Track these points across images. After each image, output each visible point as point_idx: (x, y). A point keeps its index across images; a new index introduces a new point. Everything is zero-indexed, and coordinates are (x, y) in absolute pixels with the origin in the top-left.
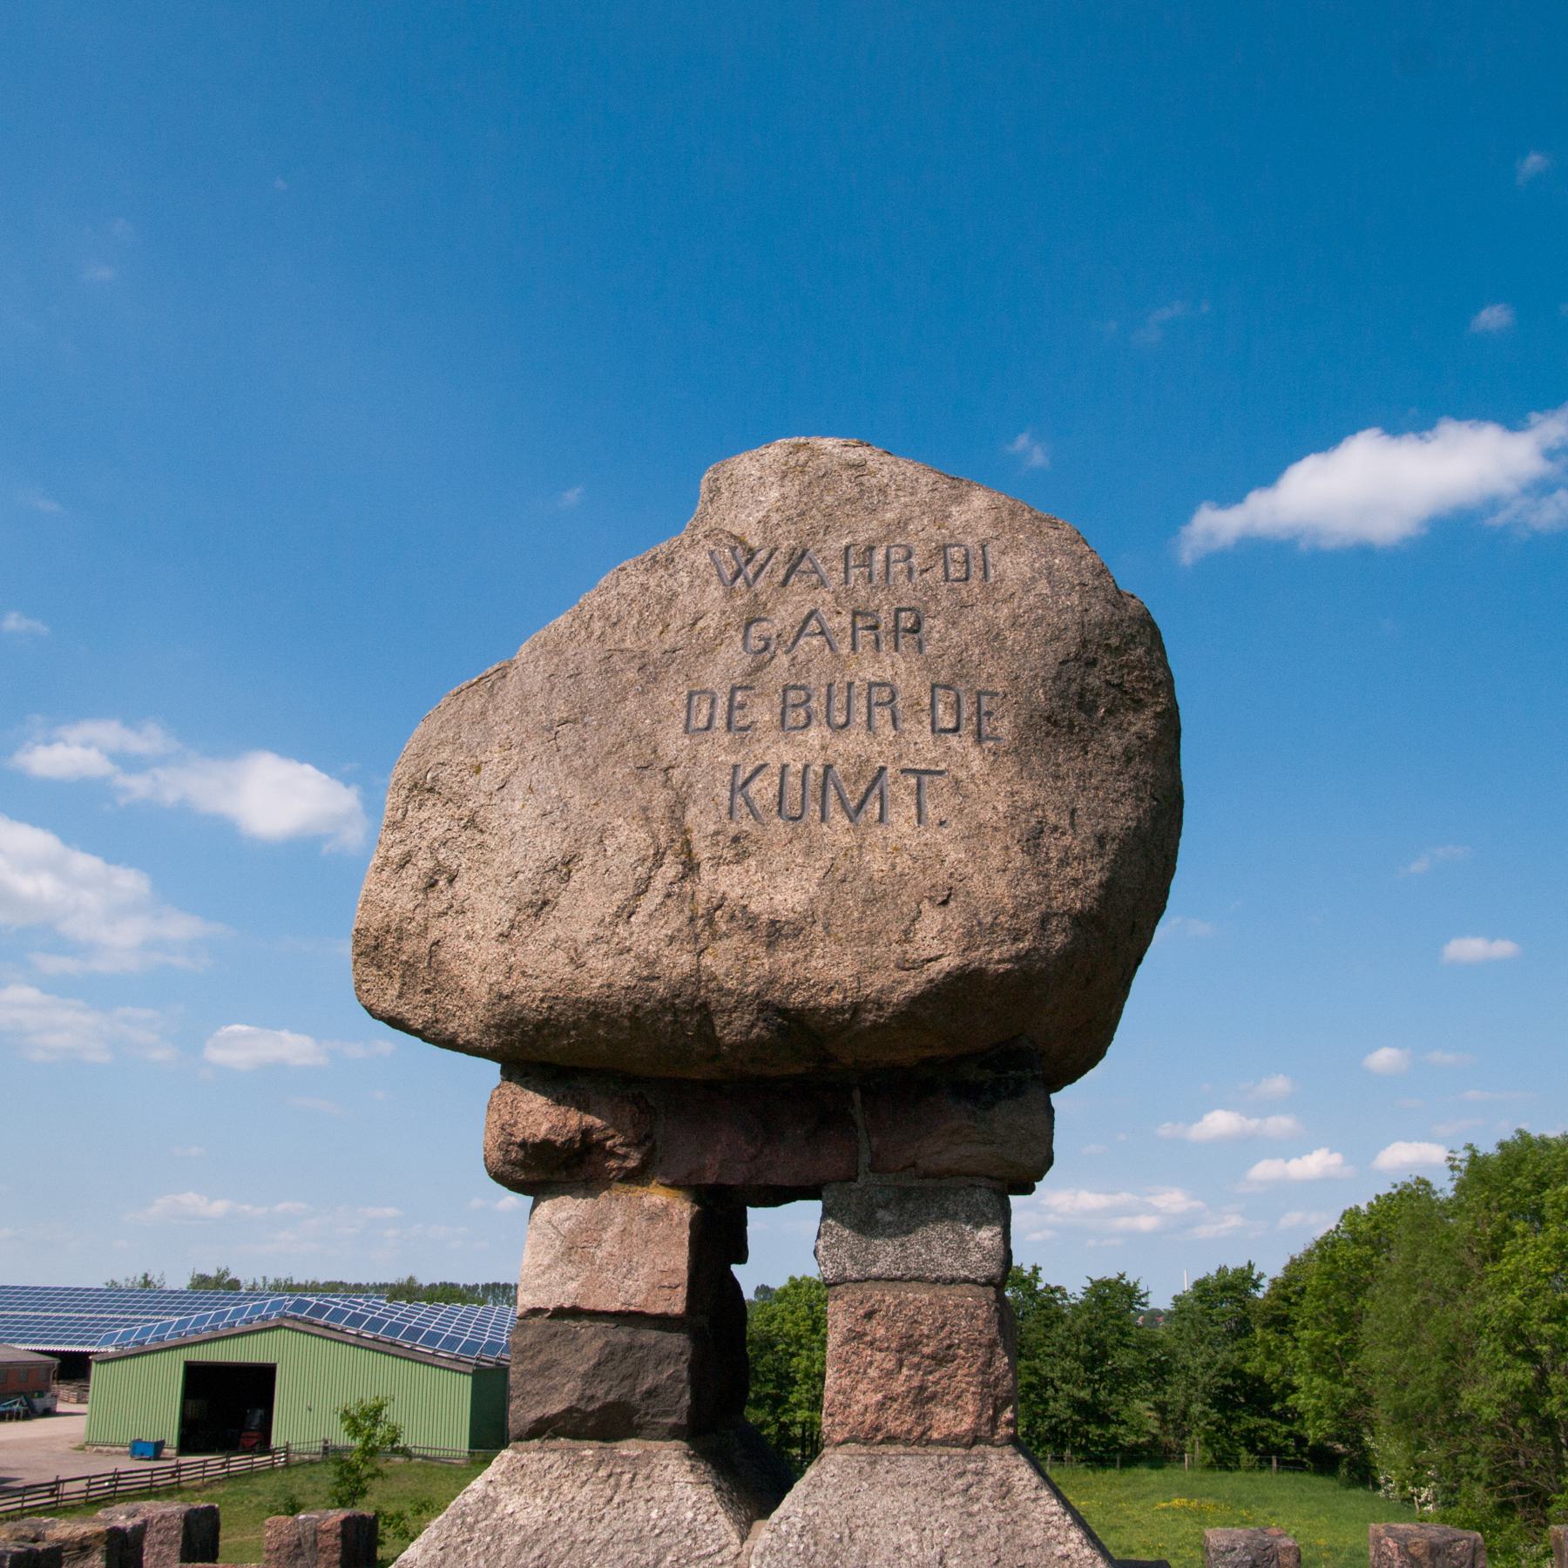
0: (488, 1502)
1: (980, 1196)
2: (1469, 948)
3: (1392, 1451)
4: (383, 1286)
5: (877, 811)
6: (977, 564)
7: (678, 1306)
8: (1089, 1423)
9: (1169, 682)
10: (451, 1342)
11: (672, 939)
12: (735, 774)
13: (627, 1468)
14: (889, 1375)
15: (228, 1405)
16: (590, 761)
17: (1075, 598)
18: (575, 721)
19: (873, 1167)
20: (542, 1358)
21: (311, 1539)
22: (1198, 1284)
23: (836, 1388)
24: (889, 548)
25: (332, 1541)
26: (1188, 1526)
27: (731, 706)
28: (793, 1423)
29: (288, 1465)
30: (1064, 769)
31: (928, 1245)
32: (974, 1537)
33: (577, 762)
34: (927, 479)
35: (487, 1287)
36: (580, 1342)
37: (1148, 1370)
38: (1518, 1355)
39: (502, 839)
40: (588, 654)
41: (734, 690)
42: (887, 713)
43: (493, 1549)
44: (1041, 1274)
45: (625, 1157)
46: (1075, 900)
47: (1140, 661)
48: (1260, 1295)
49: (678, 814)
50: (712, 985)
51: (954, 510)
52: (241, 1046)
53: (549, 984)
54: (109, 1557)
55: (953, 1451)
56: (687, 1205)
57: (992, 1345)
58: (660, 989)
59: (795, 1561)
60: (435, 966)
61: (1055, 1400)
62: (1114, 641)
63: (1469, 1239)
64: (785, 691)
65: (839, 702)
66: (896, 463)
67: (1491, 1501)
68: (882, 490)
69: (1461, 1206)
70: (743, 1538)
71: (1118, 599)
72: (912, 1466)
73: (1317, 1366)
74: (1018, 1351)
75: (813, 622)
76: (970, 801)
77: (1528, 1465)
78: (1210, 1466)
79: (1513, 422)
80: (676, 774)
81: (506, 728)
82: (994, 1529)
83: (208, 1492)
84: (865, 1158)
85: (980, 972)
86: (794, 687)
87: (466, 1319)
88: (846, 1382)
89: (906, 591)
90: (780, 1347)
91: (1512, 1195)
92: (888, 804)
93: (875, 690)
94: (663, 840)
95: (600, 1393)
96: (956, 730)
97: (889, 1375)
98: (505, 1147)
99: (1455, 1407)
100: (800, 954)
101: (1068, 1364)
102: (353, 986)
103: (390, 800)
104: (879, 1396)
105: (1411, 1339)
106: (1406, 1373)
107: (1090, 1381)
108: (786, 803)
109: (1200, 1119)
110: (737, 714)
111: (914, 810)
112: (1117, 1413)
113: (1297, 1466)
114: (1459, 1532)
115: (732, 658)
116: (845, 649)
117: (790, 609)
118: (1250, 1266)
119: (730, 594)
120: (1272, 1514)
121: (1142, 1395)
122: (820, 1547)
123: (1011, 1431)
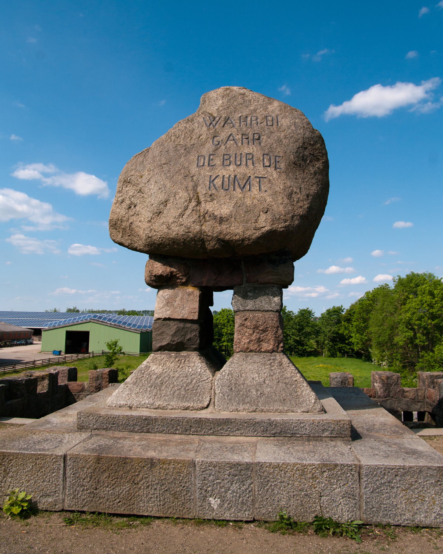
0: (147, 367)
1: (275, 289)
2: (400, 224)
3: (376, 353)
4: (116, 311)
5: (248, 188)
6: (275, 121)
7: (196, 318)
8: (299, 346)
9: (326, 154)
10: (134, 325)
11: (194, 222)
12: (210, 178)
13: (183, 358)
14: (251, 335)
15: (77, 342)
16: (172, 174)
17: (302, 131)
18: (167, 164)
19: (247, 282)
20: (161, 331)
21: (101, 375)
22: (327, 311)
23: (237, 338)
24: (251, 117)
25: (106, 376)
26: (324, 371)
27: (209, 159)
28: (223, 346)
29: (93, 357)
30: (298, 177)
31: (261, 302)
32: (273, 376)
33: (168, 175)
34: (262, 98)
35: (143, 311)
36: (171, 327)
37: (314, 332)
38: (409, 329)
39: (148, 196)
40: (171, 145)
41: (210, 155)
42: (251, 161)
43: (149, 379)
44: (287, 308)
45: (182, 279)
46: (301, 212)
47: (319, 148)
48: (343, 313)
49: (195, 189)
50: (205, 234)
51: (269, 106)
52: (77, 249)
53: (162, 234)
54: (49, 380)
55: (267, 354)
56: (198, 291)
57: (278, 327)
58: (191, 235)
59: (227, 382)
60: (131, 229)
61: (290, 340)
62: (312, 142)
63: (398, 300)
64: (224, 155)
65: (238, 158)
66: (253, 94)
67: (401, 365)
68: (250, 101)
69: (396, 291)
70: (213, 376)
71: (313, 131)
72: (257, 358)
73: (358, 331)
74: (283, 328)
75: (231, 137)
76: (273, 185)
77: (411, 356)
78: (329, 356)
79: (417, 83)
80: (195, 178)
81: (149, 165)
82: (278, 374)
83: (73, 363)
84: (245, 279)
85: (276, 231)
86: (226, 155)
87: (138, 320)
88: (240, 336)
89: (256, 129)
90: (220, 326)
91: (409, 288)
92: (251, 186)
93: (248, 155)
94: (191, 196)
95: (176, 340)
96: (269, 166)
97: (251, 335)
98: (150, 276)
99: (392, 342)
100: (228, 226)
101: (293, 331)
102: (109, 235)
103: (118, 185)
104: (248, 340)
105: (382, 325)
106: (380, 333)
107: (299, 335)
108: (224, 186)
109: (329, 268)
110: (211, 162)
111: (258, 188)
112: (306, 343)
113: (350, 356)
114: (394, 374)
115: (209, 146)
116: (240, 144)
117: (225, 133)
118: (342, 306)
119: (209, 129)
120: (345, 368)
121: (313, 339)
122: (233, 378)
123: (282, 349)
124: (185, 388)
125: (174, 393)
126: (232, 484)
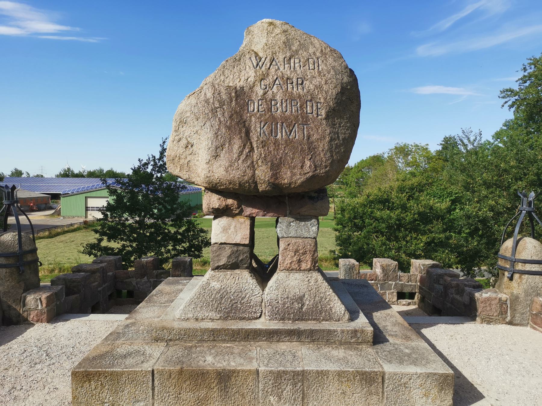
70: (263, 291)
124: (241, 302)
125: (232, 305)
126: (287, 386)
